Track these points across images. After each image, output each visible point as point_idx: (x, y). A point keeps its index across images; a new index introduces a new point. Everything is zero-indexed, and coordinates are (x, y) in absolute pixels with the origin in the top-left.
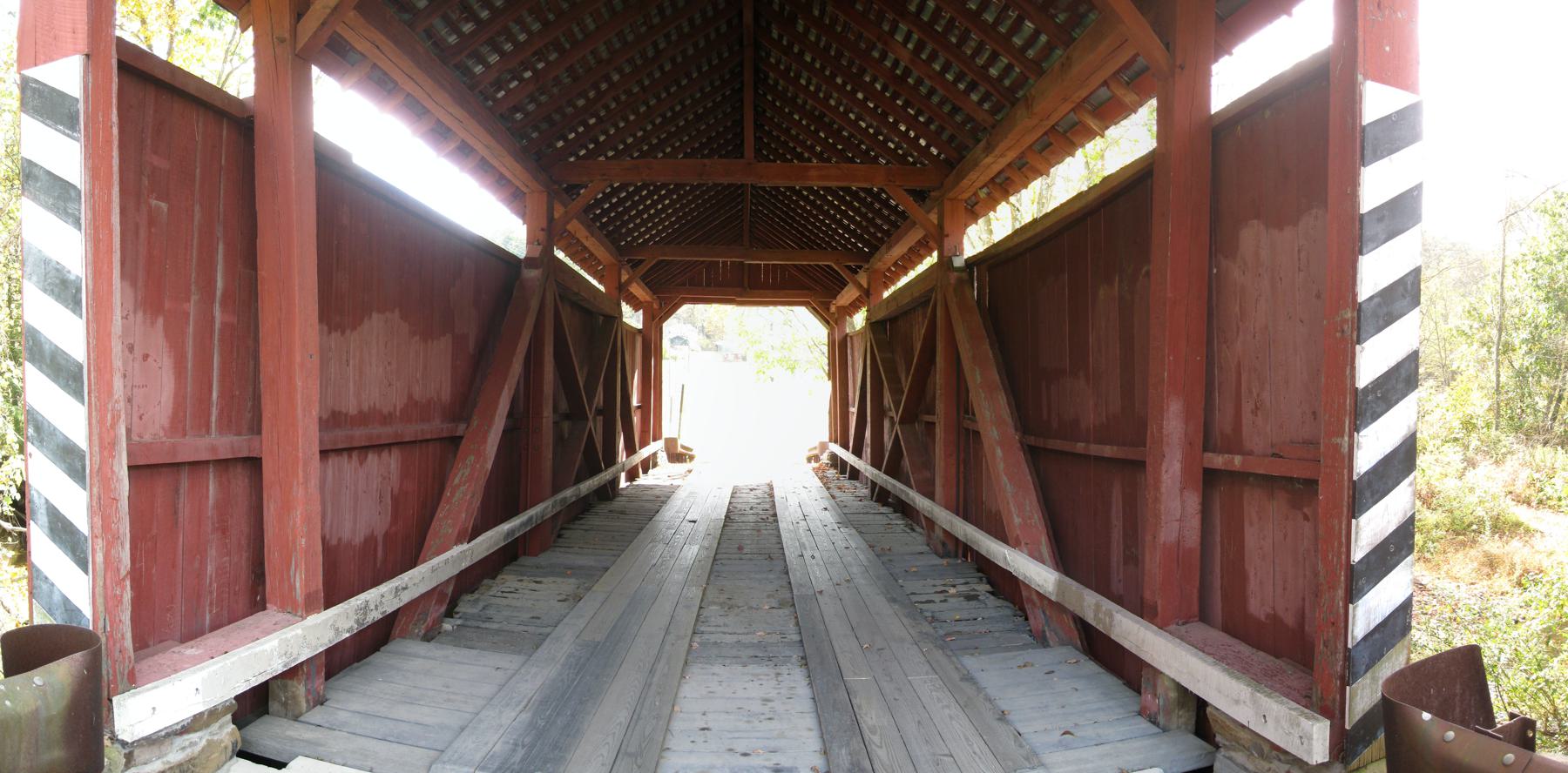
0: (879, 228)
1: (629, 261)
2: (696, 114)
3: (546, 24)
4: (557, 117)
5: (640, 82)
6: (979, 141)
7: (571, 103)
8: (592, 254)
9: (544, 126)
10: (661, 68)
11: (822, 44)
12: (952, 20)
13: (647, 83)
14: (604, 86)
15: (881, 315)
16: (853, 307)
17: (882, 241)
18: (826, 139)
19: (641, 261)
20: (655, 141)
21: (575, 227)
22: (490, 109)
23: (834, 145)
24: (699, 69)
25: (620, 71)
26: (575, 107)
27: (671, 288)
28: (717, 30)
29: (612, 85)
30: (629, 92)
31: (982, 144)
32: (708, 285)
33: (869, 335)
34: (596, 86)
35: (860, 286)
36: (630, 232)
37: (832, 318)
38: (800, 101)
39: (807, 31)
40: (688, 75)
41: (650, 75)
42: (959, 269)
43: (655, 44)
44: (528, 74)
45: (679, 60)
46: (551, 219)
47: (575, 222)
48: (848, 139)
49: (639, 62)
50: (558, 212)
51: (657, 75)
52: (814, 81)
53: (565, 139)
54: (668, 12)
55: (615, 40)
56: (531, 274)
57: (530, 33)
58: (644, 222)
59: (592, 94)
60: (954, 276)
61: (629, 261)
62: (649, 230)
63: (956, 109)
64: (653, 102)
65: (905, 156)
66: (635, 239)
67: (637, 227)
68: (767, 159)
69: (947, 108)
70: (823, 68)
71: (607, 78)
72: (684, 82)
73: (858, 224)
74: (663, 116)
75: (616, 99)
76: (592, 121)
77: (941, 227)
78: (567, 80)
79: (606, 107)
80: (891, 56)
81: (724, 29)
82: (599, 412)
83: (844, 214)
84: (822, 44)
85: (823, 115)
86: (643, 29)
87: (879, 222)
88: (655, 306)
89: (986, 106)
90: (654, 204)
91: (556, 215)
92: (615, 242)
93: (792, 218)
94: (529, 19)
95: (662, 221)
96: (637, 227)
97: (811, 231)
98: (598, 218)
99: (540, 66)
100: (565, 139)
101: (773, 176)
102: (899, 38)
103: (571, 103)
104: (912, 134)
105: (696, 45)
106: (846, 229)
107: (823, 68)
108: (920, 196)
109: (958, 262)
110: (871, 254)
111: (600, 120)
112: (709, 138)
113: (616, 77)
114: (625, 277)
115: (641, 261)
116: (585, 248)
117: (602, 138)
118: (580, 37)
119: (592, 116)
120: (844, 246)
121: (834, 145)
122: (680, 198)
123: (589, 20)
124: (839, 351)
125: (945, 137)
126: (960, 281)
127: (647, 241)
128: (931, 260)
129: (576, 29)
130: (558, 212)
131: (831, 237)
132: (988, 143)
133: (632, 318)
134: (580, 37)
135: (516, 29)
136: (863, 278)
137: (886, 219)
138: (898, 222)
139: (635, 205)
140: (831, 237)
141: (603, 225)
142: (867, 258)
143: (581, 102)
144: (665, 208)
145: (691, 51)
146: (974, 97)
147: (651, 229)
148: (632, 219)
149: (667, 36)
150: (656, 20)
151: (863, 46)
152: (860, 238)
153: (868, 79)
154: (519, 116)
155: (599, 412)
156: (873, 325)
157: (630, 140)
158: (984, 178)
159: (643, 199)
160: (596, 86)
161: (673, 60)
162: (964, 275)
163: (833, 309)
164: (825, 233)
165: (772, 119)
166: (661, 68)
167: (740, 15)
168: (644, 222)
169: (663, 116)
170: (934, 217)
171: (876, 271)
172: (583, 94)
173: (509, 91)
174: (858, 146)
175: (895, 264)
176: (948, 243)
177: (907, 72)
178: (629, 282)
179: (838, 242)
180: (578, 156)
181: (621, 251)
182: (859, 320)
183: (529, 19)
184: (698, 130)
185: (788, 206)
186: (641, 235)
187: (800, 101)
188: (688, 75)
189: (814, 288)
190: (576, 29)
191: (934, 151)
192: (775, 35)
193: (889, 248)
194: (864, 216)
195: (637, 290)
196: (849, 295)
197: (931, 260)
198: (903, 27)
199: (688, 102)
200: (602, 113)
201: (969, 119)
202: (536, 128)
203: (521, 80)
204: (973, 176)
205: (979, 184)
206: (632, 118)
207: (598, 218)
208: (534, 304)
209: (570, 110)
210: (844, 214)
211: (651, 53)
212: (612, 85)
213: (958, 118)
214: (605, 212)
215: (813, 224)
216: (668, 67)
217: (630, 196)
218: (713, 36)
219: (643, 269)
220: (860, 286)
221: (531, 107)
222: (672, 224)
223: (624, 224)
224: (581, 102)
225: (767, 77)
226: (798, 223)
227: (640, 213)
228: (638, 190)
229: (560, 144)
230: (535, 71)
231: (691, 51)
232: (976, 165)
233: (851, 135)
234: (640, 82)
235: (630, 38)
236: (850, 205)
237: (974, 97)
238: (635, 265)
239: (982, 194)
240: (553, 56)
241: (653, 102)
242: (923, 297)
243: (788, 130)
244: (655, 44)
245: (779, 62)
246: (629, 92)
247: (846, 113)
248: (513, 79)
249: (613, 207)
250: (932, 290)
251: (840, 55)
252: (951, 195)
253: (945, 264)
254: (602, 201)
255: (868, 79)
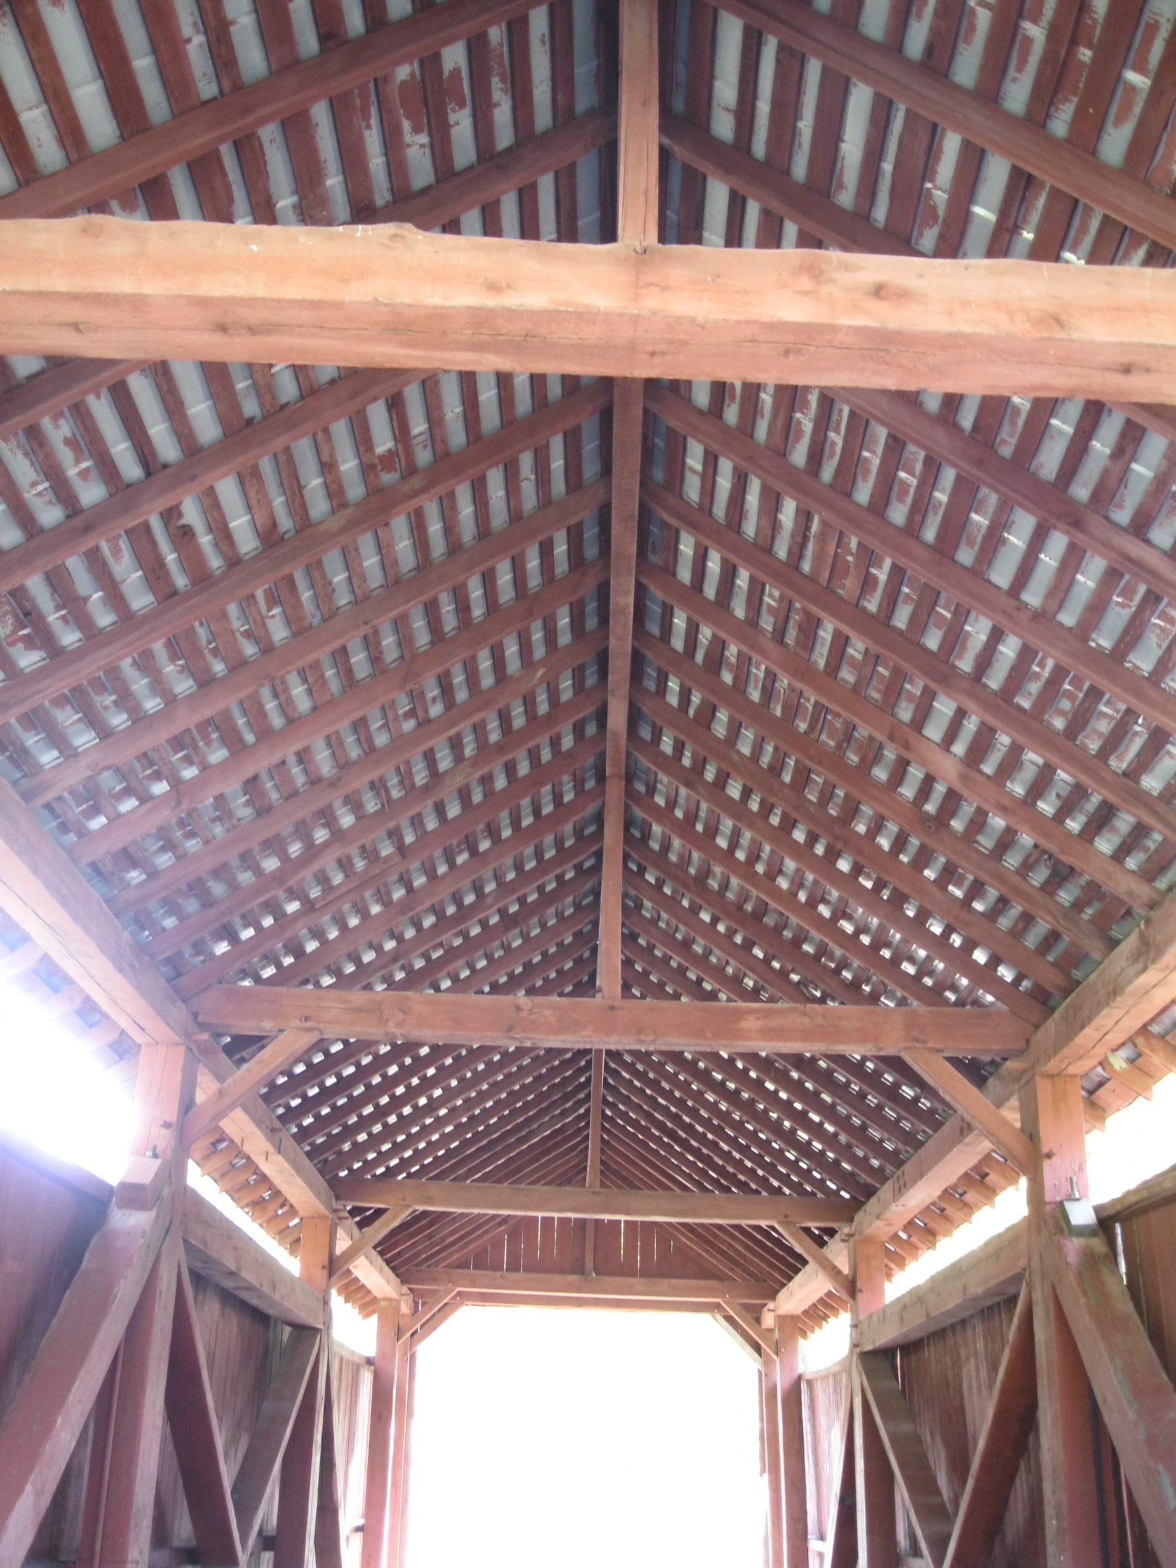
0: (876, 1147)
1: (354, 1212)
2: (503, 912)
3: (206, 681)
4: (218, 889)
5: (395, 835)
6: (1114, 944)
7: (248, 860)
8: (277, 1193)
9: (191, 906)
10: (440, 809)
11: (765, 760)
12: (1059, 673)
13: (409, 839)
14: (321, 835)
15: (887, 1335)
16: (818, 1313)
17: (881, 1176)
18: (767, 961)
19: (379, 1212)
20: (419, 964)
21: (240, 1126)
22: (70, 851)
23: (783, 974)
24: (516, 822)
25: (354, 804)
26: (258, 871)
27: (431, 1262)
28: (555, 743)
29: (338, 835)
30: (369, 853)
31: (1129, 944)
32: (513, 1267)
33: (858, 1378)
34: (303, 831)
35: (835, 1272)
36: (359, 1150)
37: (770, 1344)
38: (714, 884)
39: (735, 730)
40: (493, 832)
41: (417, 822)
42: (1082, 1231)
43: (430, 758)
44: (160, 788)
45: (477, 797)
46: (187, 1105)
47: (239, 1114)
48: (816, 958)
49: (396, 794)
50: (206, 1089)
51: (431, 824)
52: (747, 836)
53: (233, 939)
54: (461, 695)
55: (350, 740)
56: (130, 1222)
57: (170, 699)
58: (389, 1132)
59: (295, 849)
60: (1073, 1247)
61: (354, 1212)
62: (397, 1148)
63: (1061, 875)
64: (419, 881)
65: (939, 989)
66: (369, 1166)
67: (375, 1141)
68: (658, 991)
69: (1038, 877)
70: (766, 809)
71: (327, 816)
72: (485, 845)
73: (831, 1141)
74: (439, 913)
75: (345, 865)
76: (292, 907)
77: (1031, 1136)
78: (246, 813)
79: (322, 879)
80: (916, 773)
81: (567, 742)
82: (267, 1542)
83: (801, 1119)
84: (765, 760)
85: (762, 910)
86: (409, 725)
87: (876, 1134)
88: (405, 1308)
89: (1131, 863)
90: (412, 1093)
91: (200, 1097)
92: (327, 1171)
93: (689, 1129)
94: (169, 669)
95: (426, 1130)
96: (375, 1141)
97: (727, 1156)
98: (291, 1115)
99: (189, 773)
100: (233, 939)
101: (666, 1029)
102: (934, 731)
103: (248, 860)
104: (956, 940)
105: (510, 769)
106: (804, 1149)
107: (766, 809)
108: (976, 1072)
109: (1081, 1214)
110: (856, 1205)
111: (310, 906)
112: (528, 966)
113: (347, 820)
114: (343, 1244)
115: (379, 1212)
116: (264, 1178)
117: (311, 946)
118: (277, 722)
119: (292, 894)
120: (797, 1188)
121: (783, 974)
122: (465, 1085)
123: (298, 691)
124: (787, 1409)
125: (1032, 940)
126: (1090, 1260)
127: (390, 1173)
128: (1009, 1207)
129: (270, 705)
130: (206, 1089)
131: (771, 1169)
132: (1144, 940)
133: (352, 1332)
134: (277, 722)
135: (139, 684)
136: (839, 1254)
137: (892, 1127)
138: (934, 1121)
139: (372, 1093)
140: (771, 1169)
141: (304, 1134)
142: (849, 1211)
143: (271, 864)
144: (432, 1106)
145: (500, 783)
146: (1105, 845)
147: (403, 1146)
148: (364, 1123)
149: (456, 744)
150: (436, 710)
151: (853, 758)
152: (833, 1169)
153: (861, 828)
154: (135, 876)
155: (267, 1542)
156: (876, 1360)
157: (368, 957)
158: (1132, 1023)
159: (389, 1083)
160: (303, 831)
161: (464, 795)
162: (1098, 1244)
163: (768, 1320)
164: (757, 1160)
165: (654, 921)
166: (440, 809)
167: (601, 716)
168: (389, 1132)
169: (439, 913)
170: (1012, 1115)
171: (868, 1240)
172: (274, 845)
173: (115, 819)
174: (837, 972)
175: (910, 1226)
176: (1051, 1172)
177: (952, 800)
178: (350, 1254)
179: (785, 1180)
180: (258, 980)
181: (338, 1189)
182: (827, 1348)
183: (169, 669)
184: (507, 949)
185: (680, 1103)
186: (382, 1157)
187: (714, 884)
188: (493, 832)
189: (742, 1273)
190: (270, 705)
191: (1006, 973)
192: (667, 745)
193: (900, 1190)
194: (843, 1123)
195: (370, 1273)
196: (806, 1288)
197: (1009, 1207)
198: (944, 707)
199: (490, 887)
200: (315, 893)
201: (1093, 891)
202: (172, 908)
203: (145, 798)
204: (1105, 1019)
205: (1116, 1037)
206: (375, 909)
207: (291, 1115)
208: (126, 1293)
209: (245, 878)
210: (801, 1119)
211: (420, 777)
212: (338, 835)
213: (1065, 896)
214: (310, 1105)
215: (732, 1141)
216: (453, 810)
217: (363, 1073)
218: (546, 755)
219: (381, 1229)
220: (835, 1272)
221: (164, 860)
222: (446, 1139)
223: (349, 1132)
224: (271, 864)
225: (646, 836)
226: (702, 1138)
227: (381, 1113)
228: (380, 1062)
229: (222, 948)
230: (176, 783)
231: (500, 783)
232: (1115, 991)
233: (822, 950)
234: (395, 835)
235: (381, 739)
236: (812, 1099)
237: (1105, 845)
238: (366, 1220)
239: (1118, 1062)
240: (217, 755)
241: (419, 881)
242: (996, 1300)
243: (687, 944)
244: (430, 758)
245: (672, 804)
246: (369, 853)
247: (812, 903)
248: (128, 792)
249: (327, 1093)
250: (1017, 1279)
251: (803, 777)
252: (1052, 1065)
253: (1048, 1217)
254: (305, 1079)
255: (861, 828)
